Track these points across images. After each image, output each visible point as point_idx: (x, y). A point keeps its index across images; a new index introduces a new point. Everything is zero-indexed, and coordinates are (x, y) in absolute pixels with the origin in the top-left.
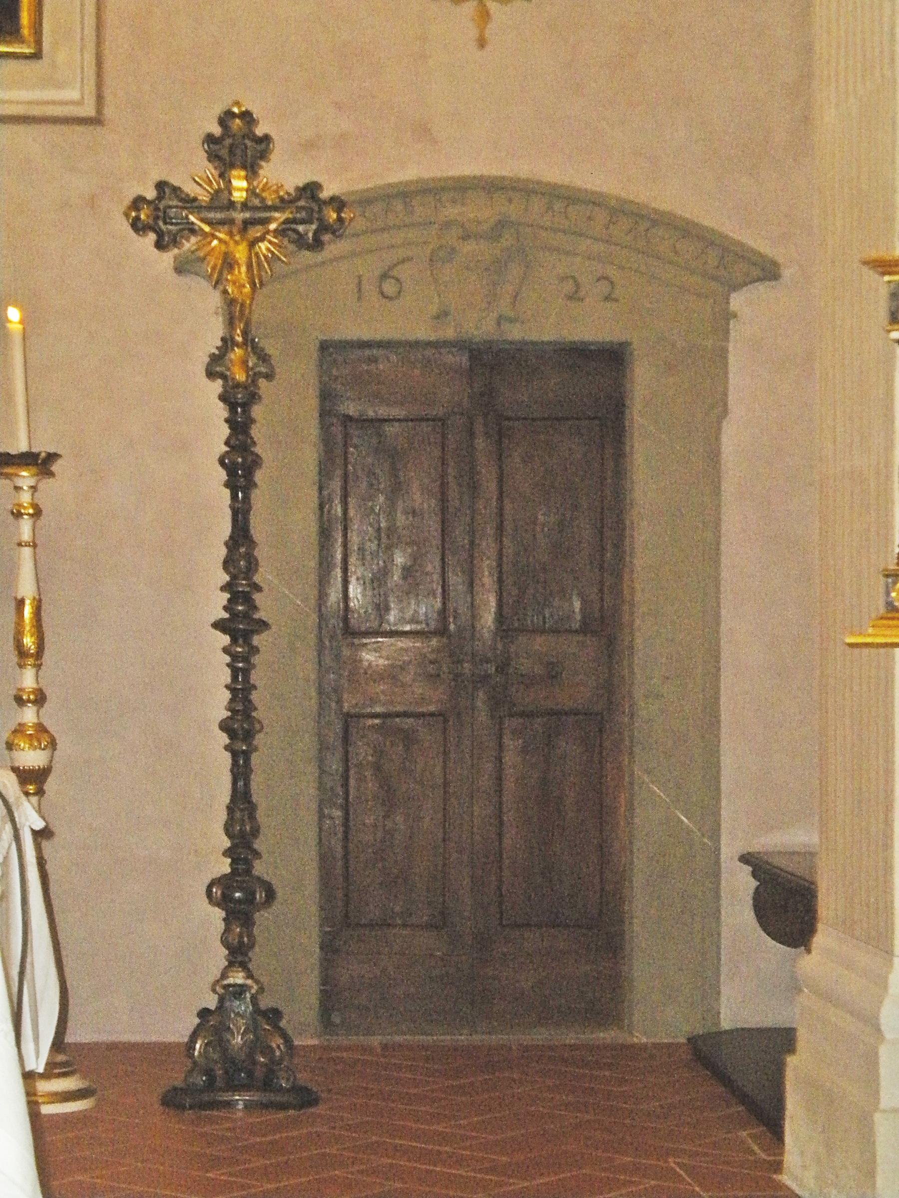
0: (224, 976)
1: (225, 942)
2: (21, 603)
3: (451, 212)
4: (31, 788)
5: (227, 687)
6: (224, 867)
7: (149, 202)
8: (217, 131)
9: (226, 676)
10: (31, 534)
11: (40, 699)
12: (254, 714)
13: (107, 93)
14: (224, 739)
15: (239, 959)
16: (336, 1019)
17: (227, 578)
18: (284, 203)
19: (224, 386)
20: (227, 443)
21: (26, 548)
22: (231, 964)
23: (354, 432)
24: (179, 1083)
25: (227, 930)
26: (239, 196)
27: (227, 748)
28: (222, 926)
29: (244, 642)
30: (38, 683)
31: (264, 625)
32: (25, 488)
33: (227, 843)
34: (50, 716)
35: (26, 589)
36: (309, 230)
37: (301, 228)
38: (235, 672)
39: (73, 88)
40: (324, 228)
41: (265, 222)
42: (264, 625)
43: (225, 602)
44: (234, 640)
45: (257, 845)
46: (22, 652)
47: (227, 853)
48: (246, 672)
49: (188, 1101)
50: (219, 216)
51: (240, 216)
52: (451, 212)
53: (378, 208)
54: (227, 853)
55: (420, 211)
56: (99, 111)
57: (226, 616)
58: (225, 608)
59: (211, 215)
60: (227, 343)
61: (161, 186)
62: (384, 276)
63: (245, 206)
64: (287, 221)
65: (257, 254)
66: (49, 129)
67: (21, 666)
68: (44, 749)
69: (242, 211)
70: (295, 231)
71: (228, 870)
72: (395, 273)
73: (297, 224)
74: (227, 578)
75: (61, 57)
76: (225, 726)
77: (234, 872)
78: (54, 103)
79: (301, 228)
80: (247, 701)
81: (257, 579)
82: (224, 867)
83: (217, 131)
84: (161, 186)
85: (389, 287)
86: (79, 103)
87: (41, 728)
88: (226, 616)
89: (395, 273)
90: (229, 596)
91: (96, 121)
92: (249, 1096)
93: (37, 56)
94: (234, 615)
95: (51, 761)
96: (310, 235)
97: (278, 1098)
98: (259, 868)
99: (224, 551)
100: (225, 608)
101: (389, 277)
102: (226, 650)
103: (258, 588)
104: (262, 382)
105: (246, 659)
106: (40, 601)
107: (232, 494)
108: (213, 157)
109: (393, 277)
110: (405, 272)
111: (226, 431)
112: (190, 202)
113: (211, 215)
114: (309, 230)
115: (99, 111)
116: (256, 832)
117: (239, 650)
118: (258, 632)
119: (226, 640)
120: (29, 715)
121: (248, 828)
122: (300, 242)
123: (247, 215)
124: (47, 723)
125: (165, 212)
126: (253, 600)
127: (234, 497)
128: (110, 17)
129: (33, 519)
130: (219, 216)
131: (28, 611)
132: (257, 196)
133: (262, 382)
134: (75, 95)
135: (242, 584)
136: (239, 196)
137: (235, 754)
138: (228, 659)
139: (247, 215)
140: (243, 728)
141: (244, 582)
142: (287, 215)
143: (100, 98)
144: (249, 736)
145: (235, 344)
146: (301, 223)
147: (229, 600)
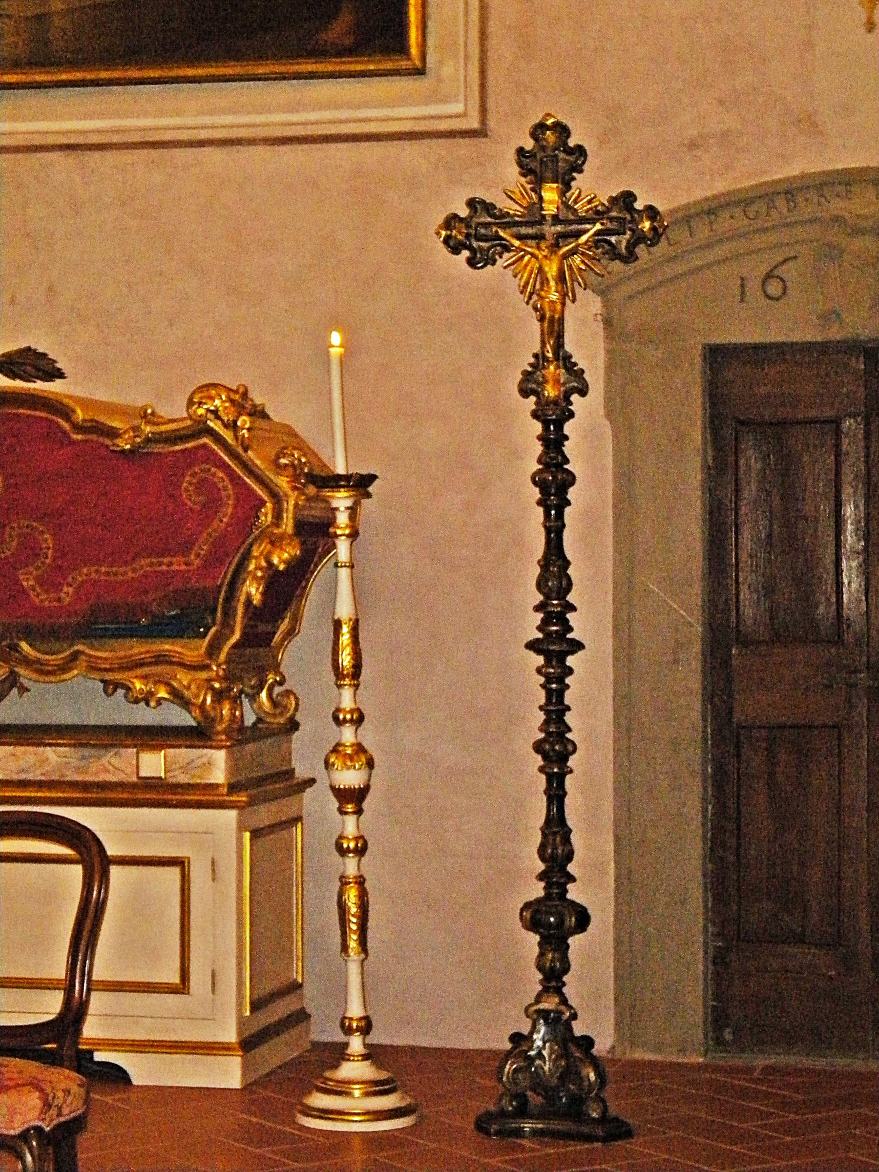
0: (538, 999)
1: (540, 968)
2: (338, 625)
3: (837, 206)
4: (350, 808)
5: (541, 708)
6: (538, 890)
7: (461, 220)
8: (529, 144)
9: (541, 697)
10: (348, 555)
11: (359, 720)
12: (569, 736)
13: (491, 104)
14: (539, 760)
15: (554, 984)
16: (728, 1035)
17: (541, 598)
18: (598, 215)
19: (537, 403)
20: (539, 461)
21: (344, 569)
22: (546, 990)
23: (834, 425)
24: (492, 1108)
25: (541, 955)
26: (550, 209)
27: (541, 770)
28: (536, 950)
29: (558, 662)
30: (355, 702)
31: (577, 646)
32: (342, 509)
33: (541, 866)
34: (368, 736)
35: (344, 610)
36: (622, 241)
37: (613, 239)
38: (549, 693)
39: (457, 101)
40: (639, 238)
41: (578, 234)
42: (577, 646)
43: (539, 622)
44: (548, 663)
45: (571, 868)
46: (338, 673)
47: (541, 877)
48: (560, 694)
49: (494, 1128)
50: (530, 231)
51: (550, 230)
52: (837, 206)
53: (760, 207)
54: (541, 877)
55: (807, 210)
56: (483, 121)
57: (540, 635)
58: (539, 628)
59: (524, 230)
60: (540, 360)
61: (471, 203)
62: (769, 276)
63: (556, 220)
64: (597, 233)
65: (570, 267)
66: (433, 143)
67: (339, 687)
68: (359, 769)
69: (554, 225)
70: (609, 243)
71: (541, 893)
72: (776, 273)
73: (608, 235)
74: (541, 598)
75: (447, 70)
76: (538, 747)
77: (548, 896)
78: (439, 117)
79: (613, 239)
80: (561, 721)
81: (570, 598)
82: (538, 890)
83: (529, 144)
84: (471, 203)
85: (774, 288)
86: (465, 115)
87: (360, 749)
88: (540, 635)
89: (776, 273)
90: (542, 615)
91: (480, 133)
92: (544, 1124)
93: (420, 72)
94: (548, 635)
95: (369, 780)
96: (624, 244)
97: (585, 1129)
98: (573, 893)
99: (537, 571)
100: (539, 628)
101: (773, 277)
102: (539, 671)
103: (572, 608)
104: (575, 398)
105: (560, 680)
106: (357, 621)
107: (544, 512)
108: (526, 171)
109: (778, 277)
110: (789, 272)
111: (538, 448)
112: (504, 220)
113: (524, 230)
114: (622, 241)
115: (483, 121)
116: (569, 856)
117: (552, 670)
118: (572, 653)
119: (540, 660)
120: (348, 735)
121: (560, 851)
122: (614, 253)
123: (559, 228)
124: (366, 745)
125: (476, 230)
126: (567, 621)
127: (547, 515)
128: (493, 27)
129: (351, 540)
130: (530, 231)
131: (345, 629)
132: (569, 208)
133: (575, 398)
134: (459, 108)
135: (553, 605)
136: (550, 209)
137: (550, 778)
138: (542, 680)
139: (559, 228)
140: (554, 750)
141: (555, 602)
142: (598, 226)
143: (483, 110)
144: (563, 758)
145: (545, 359)
146: (613, 235)
147: (543, 620)
